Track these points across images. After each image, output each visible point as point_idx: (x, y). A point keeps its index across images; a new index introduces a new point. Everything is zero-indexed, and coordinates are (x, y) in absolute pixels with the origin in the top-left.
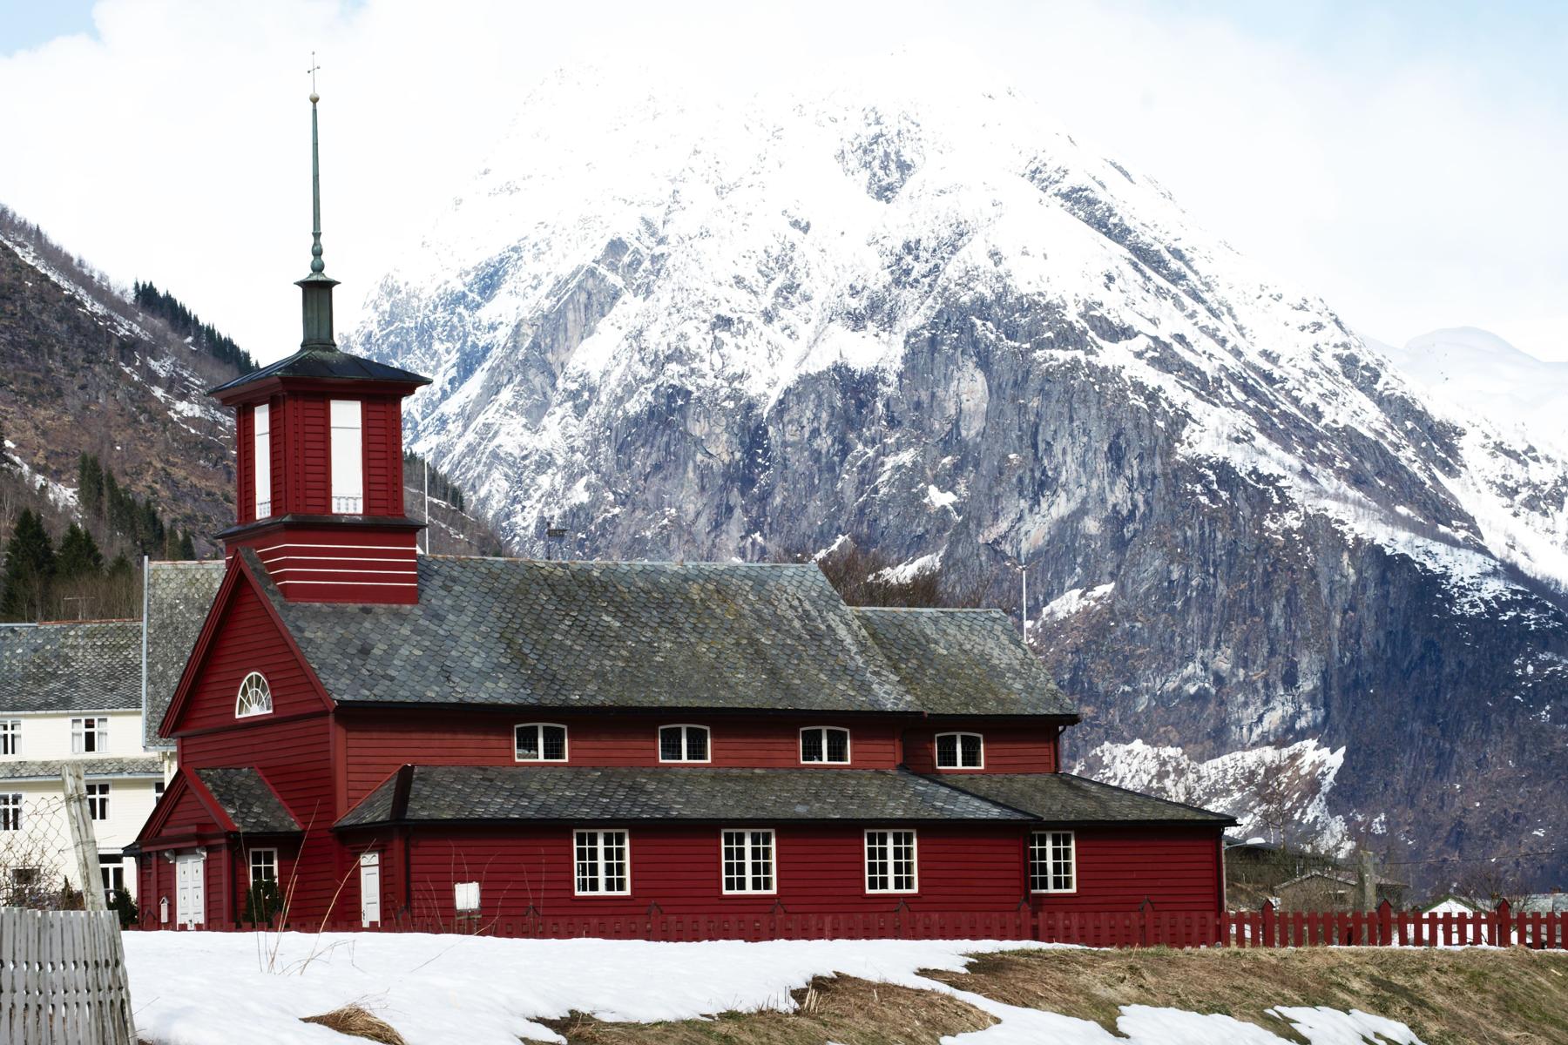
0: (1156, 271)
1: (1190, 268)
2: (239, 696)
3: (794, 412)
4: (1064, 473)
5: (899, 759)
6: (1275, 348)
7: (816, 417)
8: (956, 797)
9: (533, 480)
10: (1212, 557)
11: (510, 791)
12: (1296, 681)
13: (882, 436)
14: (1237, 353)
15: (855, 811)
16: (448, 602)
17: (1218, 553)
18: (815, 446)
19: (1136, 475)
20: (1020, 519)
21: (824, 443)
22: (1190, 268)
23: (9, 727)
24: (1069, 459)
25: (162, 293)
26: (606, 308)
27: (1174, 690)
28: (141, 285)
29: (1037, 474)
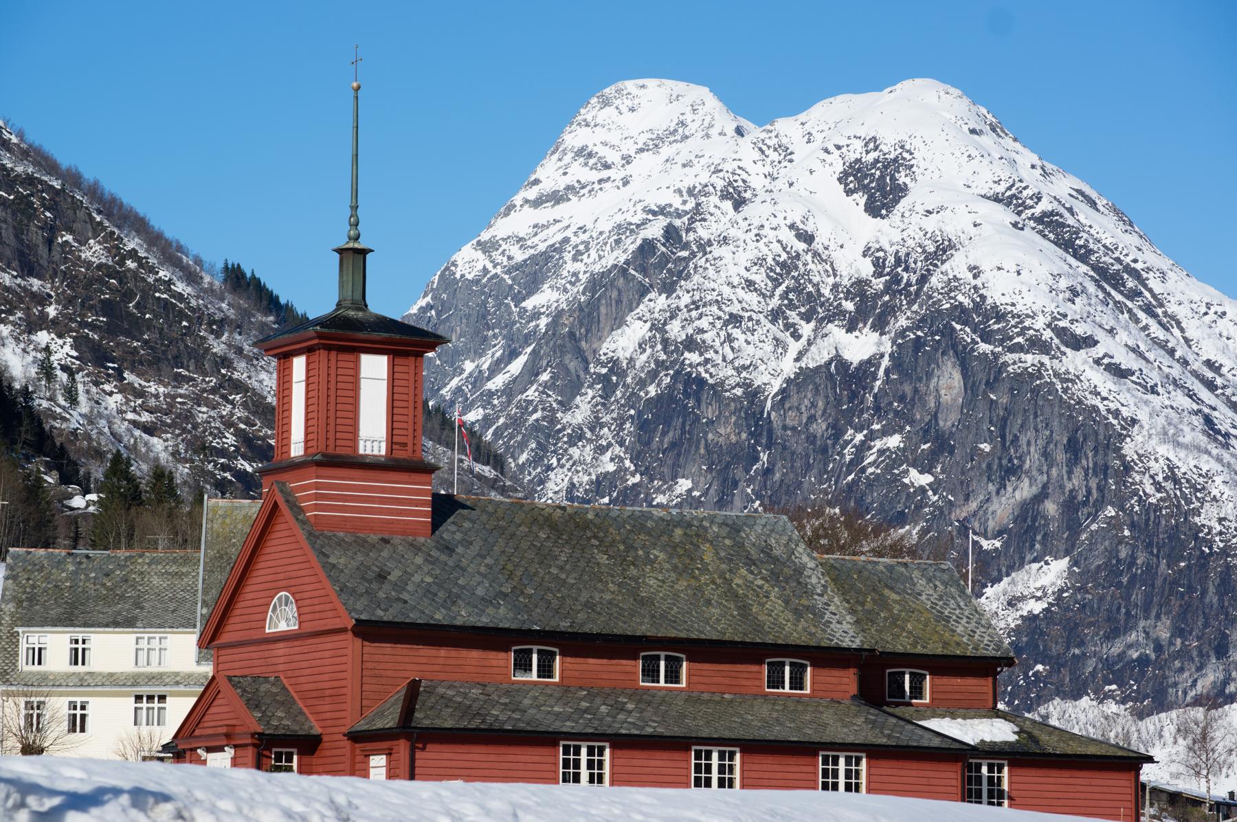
0: (1115, 287)
1: (1145, 286)
2: (270, 613)
3: (794, 400)
4: (1028, 462)
5: (853, 689)
6: (1219, 358)
7: (814, 405)
8: (903, 727)
9: (566, 450)
10: (1155, 540)
11: (506, 704)
12: (1227, 652)
13: (870, 424)
14: (1185, 363)
15: (810, 734)
16: (458, 536)
17: (1161, 536)
18: (811, 430)
19: (1091, 465)
20: (988, 500)
21: (820, 427)
22: (1145, 286)
23: (80, 642)
24: (1032, 449)
25: (283, 301)
26: (634, 305)
27: (1119, 655)
28: (230, 266)
29: (1004, 462)
